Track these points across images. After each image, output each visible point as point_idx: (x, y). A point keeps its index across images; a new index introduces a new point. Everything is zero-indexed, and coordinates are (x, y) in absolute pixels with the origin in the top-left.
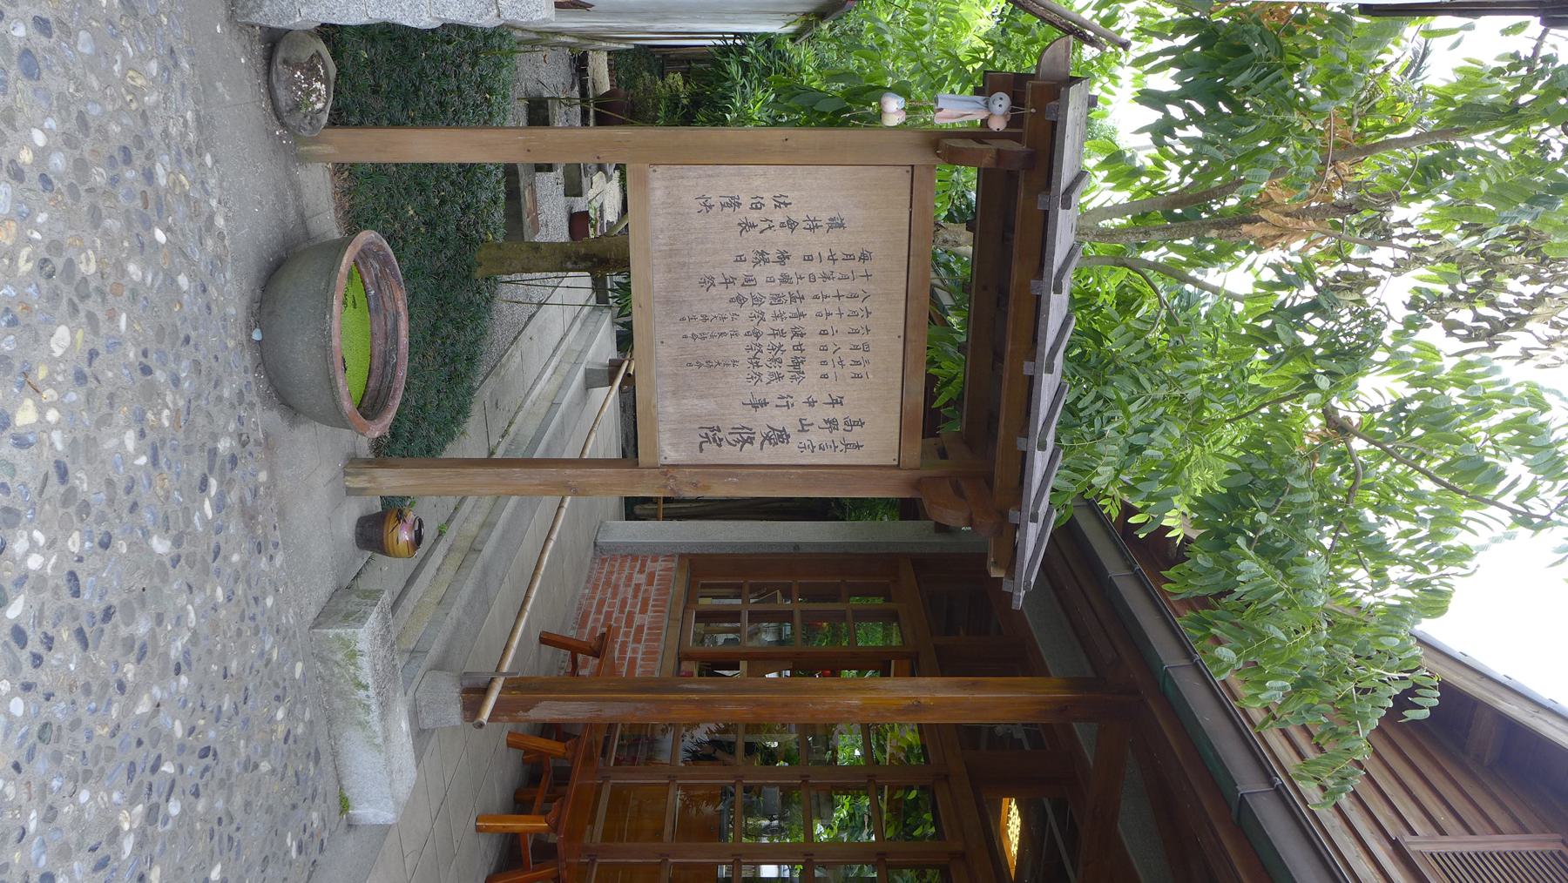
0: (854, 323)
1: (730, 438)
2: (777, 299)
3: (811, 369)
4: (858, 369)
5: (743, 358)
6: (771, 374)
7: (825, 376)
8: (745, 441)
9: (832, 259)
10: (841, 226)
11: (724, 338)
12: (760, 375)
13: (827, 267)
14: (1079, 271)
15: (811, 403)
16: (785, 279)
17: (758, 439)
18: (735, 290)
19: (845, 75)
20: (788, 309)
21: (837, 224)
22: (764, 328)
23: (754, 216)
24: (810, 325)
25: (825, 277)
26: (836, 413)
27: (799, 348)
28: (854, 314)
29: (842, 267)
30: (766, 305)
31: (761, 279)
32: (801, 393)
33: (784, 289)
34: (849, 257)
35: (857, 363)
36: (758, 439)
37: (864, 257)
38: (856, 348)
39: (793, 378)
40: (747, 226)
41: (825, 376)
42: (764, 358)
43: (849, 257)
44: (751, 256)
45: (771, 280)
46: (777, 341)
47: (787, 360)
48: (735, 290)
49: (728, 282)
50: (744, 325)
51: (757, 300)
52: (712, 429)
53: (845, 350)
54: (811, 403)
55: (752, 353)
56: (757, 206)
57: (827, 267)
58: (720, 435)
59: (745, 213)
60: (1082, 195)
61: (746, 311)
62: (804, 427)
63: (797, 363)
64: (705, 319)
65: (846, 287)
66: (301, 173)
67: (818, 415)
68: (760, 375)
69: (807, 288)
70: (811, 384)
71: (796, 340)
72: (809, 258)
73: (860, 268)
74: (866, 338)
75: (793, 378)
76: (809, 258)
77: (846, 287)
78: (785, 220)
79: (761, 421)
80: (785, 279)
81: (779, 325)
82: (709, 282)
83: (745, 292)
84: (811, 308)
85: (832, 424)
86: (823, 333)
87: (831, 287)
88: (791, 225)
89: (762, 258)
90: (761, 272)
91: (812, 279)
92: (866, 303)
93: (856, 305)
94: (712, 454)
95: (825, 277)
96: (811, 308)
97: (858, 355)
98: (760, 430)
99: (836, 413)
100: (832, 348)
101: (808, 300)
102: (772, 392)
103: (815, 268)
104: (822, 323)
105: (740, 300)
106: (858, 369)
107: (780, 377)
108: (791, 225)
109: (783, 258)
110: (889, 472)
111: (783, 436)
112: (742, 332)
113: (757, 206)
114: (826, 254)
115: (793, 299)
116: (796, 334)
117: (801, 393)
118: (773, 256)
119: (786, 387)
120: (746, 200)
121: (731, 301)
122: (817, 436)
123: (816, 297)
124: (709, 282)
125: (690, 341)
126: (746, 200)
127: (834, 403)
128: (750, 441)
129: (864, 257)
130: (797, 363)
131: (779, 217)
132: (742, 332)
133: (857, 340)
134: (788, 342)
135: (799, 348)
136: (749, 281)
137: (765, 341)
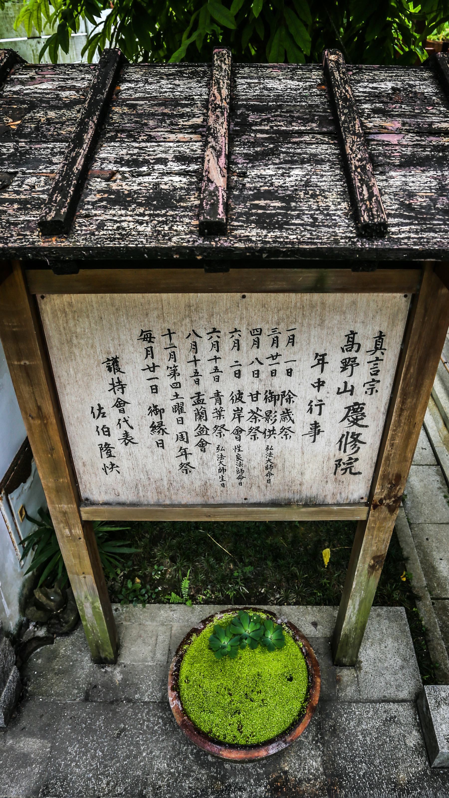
0: (227, 343)
3: (280, 384)
4: (283, 339)
5: (261, 443)
6: (283, 419)
7: (289, 372)
9: (153, 368)
10: (115, 361)
11: (225, 478)
12: (283, 429)
13: (162, 373)
14: (188, 22)
16: (179, 408)
17: (355, 429)
18: (192, 447)
19: (295, 161)
20: (211, 406)
21: (114, 364)
25: (174, 373)
26: (335, 359)
28: (217, 346)
30: (207, 424)
32: (304, 392)
36: (355, 429)
42: (263, 425)
44: (157, 436)
46: (246, 414)
48: (192, 447)
49: (184, 453)
50: (230, 440)
56: (107, 431)
57: (162, 373)
63: (271, 397)
64: (222, 470)
67: (334, 377)
68: (283, 429)
69: (187, 391)
71: (246, 398)
72: (155, 389)
74: (244, 332)
75: (289, 400)
76: (155, 389)
78: (116, 410)
81: (229, 414)
82: (186, 468)
84: (208, 386)
85: (348, 364)
86: (238, 374)
87: (185, 370)
89: (157, 428)
90: (173, 428)
92: (202, 332)
95: (174, 373)
97: (265, 340)
101: (200, 389)
103: (165, 382)
105: (202, 445)
106: (283, 339)
110: (420, 309)
112: (237, 443)
113: (107, 431)
114: (150, 374)
122: (361, 375)
124: (186, 468)
125: (243, 481)
129: (147, 336)
131: (113, 415)
132: (237, 443)
133: (246, 341)
134: (248, 406)
135: (255, 397)
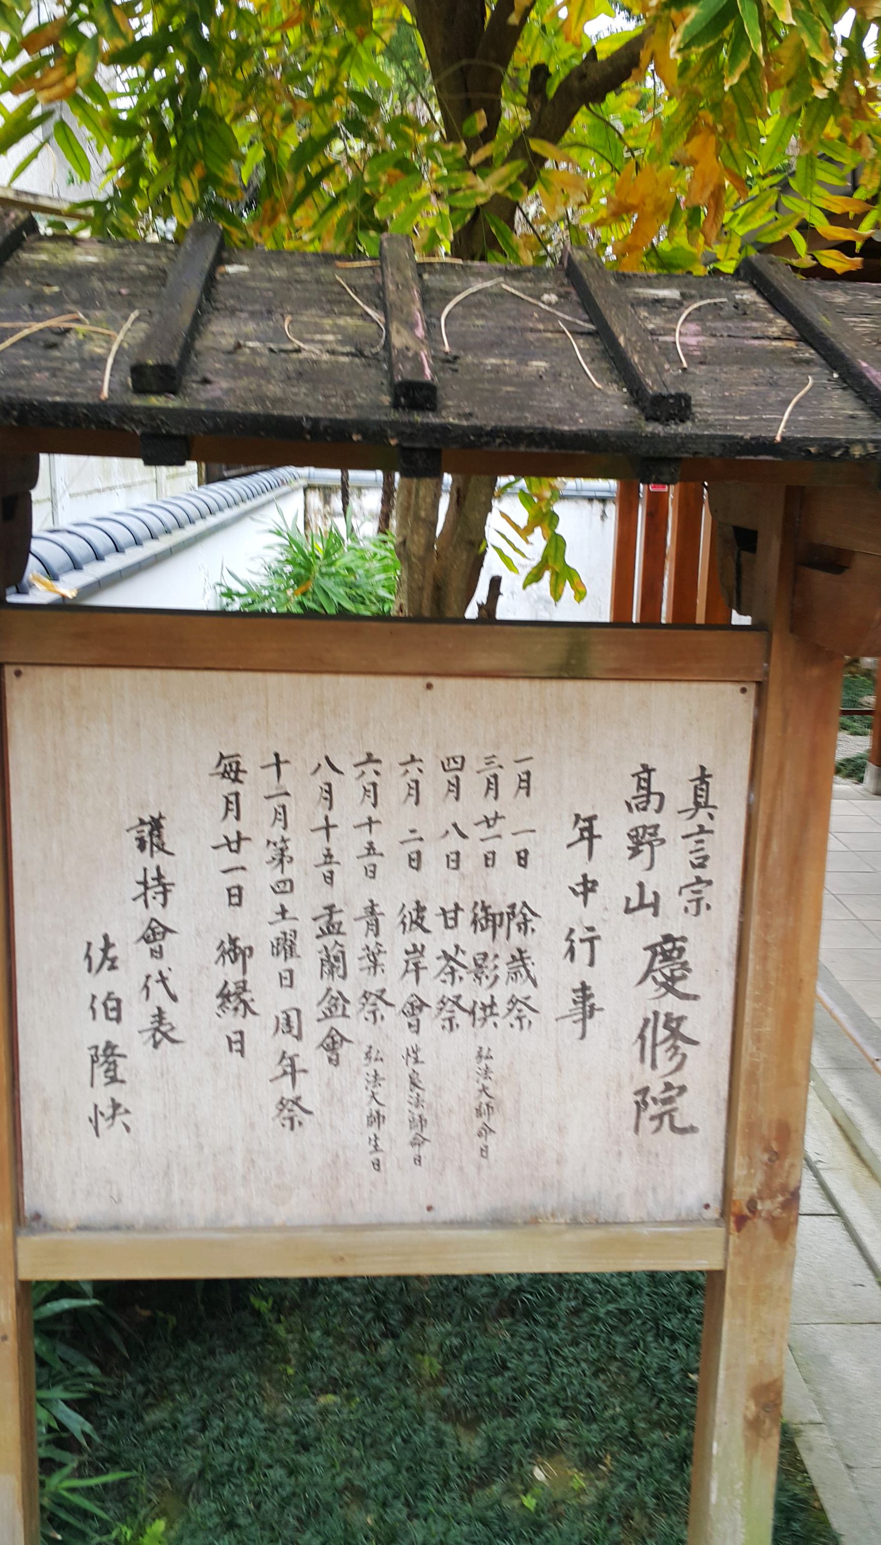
0: (394, 787)
1: (665, 1064)
2: (332, 963)
3: (505, 887)
5: (467, 1038)
7: (522, 858)
8: (675, 1034)
9: (235, 843)
10: (156, 824)
12: (513, 1001)
13: (255, 854)
15: (588, 886)
17: (671, 1004)
18: (310, 1054)
20: (355, 939)
22: (400, 991)
23: (138, 1014)
24: (395, 891)
25: (282, 858)
26: (615, 829)
27: (450, 917)
29: (257, 820)
31: (286, 999)
32: (558, 912)
33: (310, 949)
34: (233, 805)
35: (493, 784)
36: (671, 1004)
37: (231, 770)
38: (455, 787)
39: (524, 927)
40: (160, 1030)
41: (522, 858)
42: (471, 991)
43: (233, 805)
44: (232, 1022)
45: (288, 979)
46: (432, 962)
47: (481, 941)
48: (310, 1054)
50: (394, 1029)
51: (335, 1004)
52: (641, 1106)
53: (453, 811)
54: (588, 886)
55: (462, 1018)
56: (114, 1009)
58: (657, 1089)
59: (130, 1034)
60: (727, 200)
61: (356, 1027)
62: (645, 903)
63: (488, 918)
64: (377, 1119)
65: (305, 810)
66: (274, 247)
67: (617, 872)
68: (513, 1001)
69: (306, 904)
70: (545, 888)
71: (432, 920)
72: (236, 896)
73: (256, 784)
74: (431, 765)
76: (236, 896)
77: (305, 810)
78: (145, 948)
79: (626, 999)
80: (286, 946)
81: (394, 961)
82: (291, 1111)
83: (315, 1032)
84: (351, 890)
85: (641, 841)
87: (305, 848)
88: (155, 934)
89: (234, 997)
90: (269, 998)
91: (285, 887)
93: (348, 789)
94: (703, 1106)
95: (282, 858)
96: (351, 890)
98: (649, 999)
99: (615, 829)
100: (454, 842)
102: (555, 975)
103: (260, 877)
104: (392, 863)
105: (333, 1044)
107: (520, 957)
108: (155, 934)
109: (234, 951)
111: (668, 950)
112: (409, 1039)
113: (114, 1009)
114: (227, 859)
115: (331, 929)
116: (418, 923)
117: (558, 912)
118: (232, 972)
119: (545, 945)
120: (102, 1031)
121: (335, 1062)
123: (329, 878)
124: (291, 1111)
126: (102, 1031)
127: (588, 831)
128: (673, 1024)
129: (231, 770)
130: (488, 918)
131: (136, 960)
133: (434, 782)
134: (438, 940)
135: (450, 917)
136: (289, 1024)
137: (432, 988)
